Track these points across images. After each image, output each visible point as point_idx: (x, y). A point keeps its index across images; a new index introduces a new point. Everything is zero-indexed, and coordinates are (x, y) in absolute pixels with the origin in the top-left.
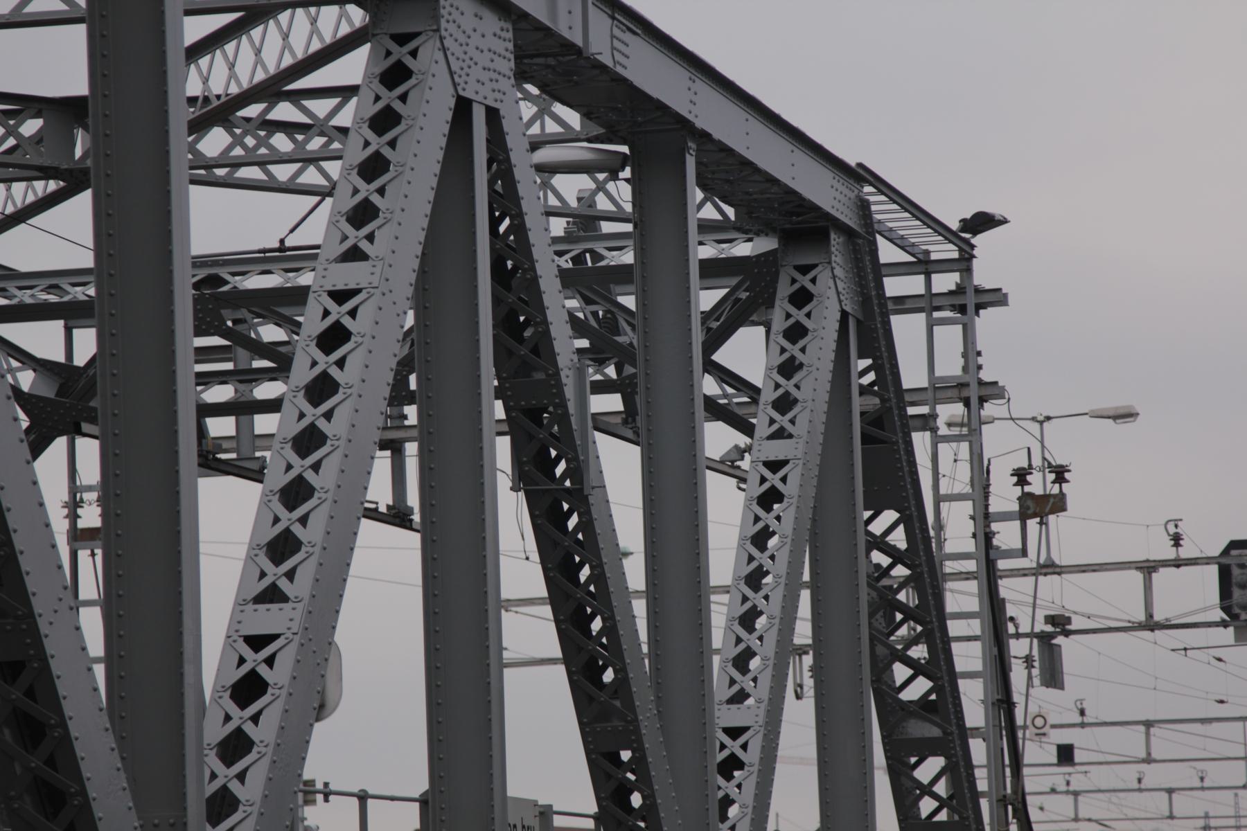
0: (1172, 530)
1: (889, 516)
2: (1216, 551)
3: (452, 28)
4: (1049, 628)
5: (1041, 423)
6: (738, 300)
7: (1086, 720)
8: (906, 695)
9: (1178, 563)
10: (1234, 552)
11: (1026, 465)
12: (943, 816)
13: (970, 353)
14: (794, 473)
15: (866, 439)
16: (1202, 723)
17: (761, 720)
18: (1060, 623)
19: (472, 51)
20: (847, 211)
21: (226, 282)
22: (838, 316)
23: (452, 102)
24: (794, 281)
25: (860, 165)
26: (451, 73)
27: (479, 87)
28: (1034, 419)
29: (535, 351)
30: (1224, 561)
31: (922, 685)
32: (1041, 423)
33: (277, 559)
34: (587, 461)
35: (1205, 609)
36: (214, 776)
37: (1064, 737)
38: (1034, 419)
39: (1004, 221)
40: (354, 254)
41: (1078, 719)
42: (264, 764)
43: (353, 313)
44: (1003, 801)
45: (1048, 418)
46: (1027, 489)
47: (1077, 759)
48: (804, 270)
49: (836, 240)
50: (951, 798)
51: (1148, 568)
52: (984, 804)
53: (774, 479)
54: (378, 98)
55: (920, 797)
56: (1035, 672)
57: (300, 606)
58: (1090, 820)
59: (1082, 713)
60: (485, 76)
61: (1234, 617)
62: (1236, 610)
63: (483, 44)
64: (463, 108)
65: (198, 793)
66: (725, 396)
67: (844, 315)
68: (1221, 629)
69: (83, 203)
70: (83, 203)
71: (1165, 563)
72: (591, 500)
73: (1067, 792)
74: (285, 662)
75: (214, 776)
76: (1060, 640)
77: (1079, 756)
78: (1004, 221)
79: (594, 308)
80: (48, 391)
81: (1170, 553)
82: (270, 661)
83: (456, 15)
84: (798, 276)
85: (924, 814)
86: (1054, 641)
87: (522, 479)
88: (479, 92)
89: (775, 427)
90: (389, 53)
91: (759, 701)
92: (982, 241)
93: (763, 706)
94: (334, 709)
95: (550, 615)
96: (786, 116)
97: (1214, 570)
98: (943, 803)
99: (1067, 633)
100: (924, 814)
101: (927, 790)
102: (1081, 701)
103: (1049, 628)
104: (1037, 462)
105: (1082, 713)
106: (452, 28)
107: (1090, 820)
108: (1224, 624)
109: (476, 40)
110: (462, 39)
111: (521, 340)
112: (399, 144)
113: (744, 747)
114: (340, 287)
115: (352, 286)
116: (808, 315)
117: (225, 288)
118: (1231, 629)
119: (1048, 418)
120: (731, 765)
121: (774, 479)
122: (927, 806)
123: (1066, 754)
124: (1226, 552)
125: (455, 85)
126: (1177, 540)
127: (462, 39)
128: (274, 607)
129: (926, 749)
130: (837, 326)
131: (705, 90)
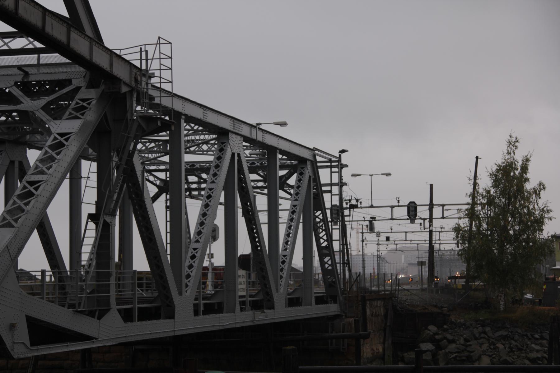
0: (398, 199)
1: (319, 212)
2: (407, 204)
3: (231, 141)
4: (371, 219)
5: (371, 176)
6: (291, 172)
7: (393, 231)
8: (323, 245)
9: (399, 206)
10: (411, 204)
11: (351, 199)
12: (330, 268)
13: (341, 178)
14: (298, 207)
15: (314, 198)
16: (362, 260)
17: (289, 254)
18: (373, 218)
19: (235, 144)
20: (311, 157)
21: (195, 166)
22: (308, 177)
23: (231, 154)
24: (300, 170)
25: (314, 148)
26: (231, 149)
27: (236, 150)
28: (370, 175)
29: (246, 193)
30: (409, 206)
31: (326, 243)
32: (371, 176)
33: (198, 235)
34: (255, 212)
35: (405, 216)
36: (187, 271)
37: (388, 235)
38: (370, 175)
39: (348, 151)
40: (213, 182)
41: (391, 231)
42: (195, 270)
43: (212, 193)
44: (344, 263)
45: (373, 175)
46: (351, 203)
47: (390, 240)
48: (302, 168)
49: (308, 163)
50: (331, 264)
51: (392, 207)
52: (338, 265)
53: (294, 209)
54: (218, 154)
55: (325, 264)
56: (368, 228)
57: (202, 244)
58: (399, 250)
59: (392, 229)
60: (237, 148)
61: (410, 218)
62: (411, 216)
63: (237, 143)
64: (233, 154)
65: (184, 274)
66: (289, 190)
67: (310, 177)
68: (407, 220)
69: (168, 156)
70: (168, 156)
71: (396, 206)
72: (256, 219)
73: (394, 244)
74: (199, 253)
75: (187, 271)
76: (374, 222)
77: (391, 239)
78: (348, 151)
79: (264, 172)
80: (162, 185)
81: (397, 204)
82: (197, 252)
83: (232, 138)
84: (301, 169)
85: (326, 267)
86: (373, 222)
87: (244, 215)
88: (236, 151)
89: (295, 198)
90: (220, 146)
91: (289, 250)
92: (343, 155)
93: (290, 251)
94: (217, 240)
95: (267, 214)
96: (297, 142)
97: (406, 208)
98: (330, 265)
99: (375, 220)
100: (326, 267)
101: (327, 263)
102: (392, 227)
103: (371, 219)
104: (353, 198)
105: (392, 229)
106: (231, 141)
107: (399, 250)
108: (408, 219)
109: (236, 142)
110: (233, 142)
111: (244, 191)
112: (217, 179)
113: (286, 259)
114: (210, 188)
115: (212, 188)
116: (303, 177)
117: (195, 167)
118: (409, 220)
119: (373, 175)
120: (283, 262)
121: (294, 209)
122: (327, 266)
123: (388, 239)
124: (409, 204)
125: (232, 151)
126: (398, 201)
127: (233, 142)
128: (198, 243)
129: (326, 255)
130: (308, 179)
131: (281, 141)
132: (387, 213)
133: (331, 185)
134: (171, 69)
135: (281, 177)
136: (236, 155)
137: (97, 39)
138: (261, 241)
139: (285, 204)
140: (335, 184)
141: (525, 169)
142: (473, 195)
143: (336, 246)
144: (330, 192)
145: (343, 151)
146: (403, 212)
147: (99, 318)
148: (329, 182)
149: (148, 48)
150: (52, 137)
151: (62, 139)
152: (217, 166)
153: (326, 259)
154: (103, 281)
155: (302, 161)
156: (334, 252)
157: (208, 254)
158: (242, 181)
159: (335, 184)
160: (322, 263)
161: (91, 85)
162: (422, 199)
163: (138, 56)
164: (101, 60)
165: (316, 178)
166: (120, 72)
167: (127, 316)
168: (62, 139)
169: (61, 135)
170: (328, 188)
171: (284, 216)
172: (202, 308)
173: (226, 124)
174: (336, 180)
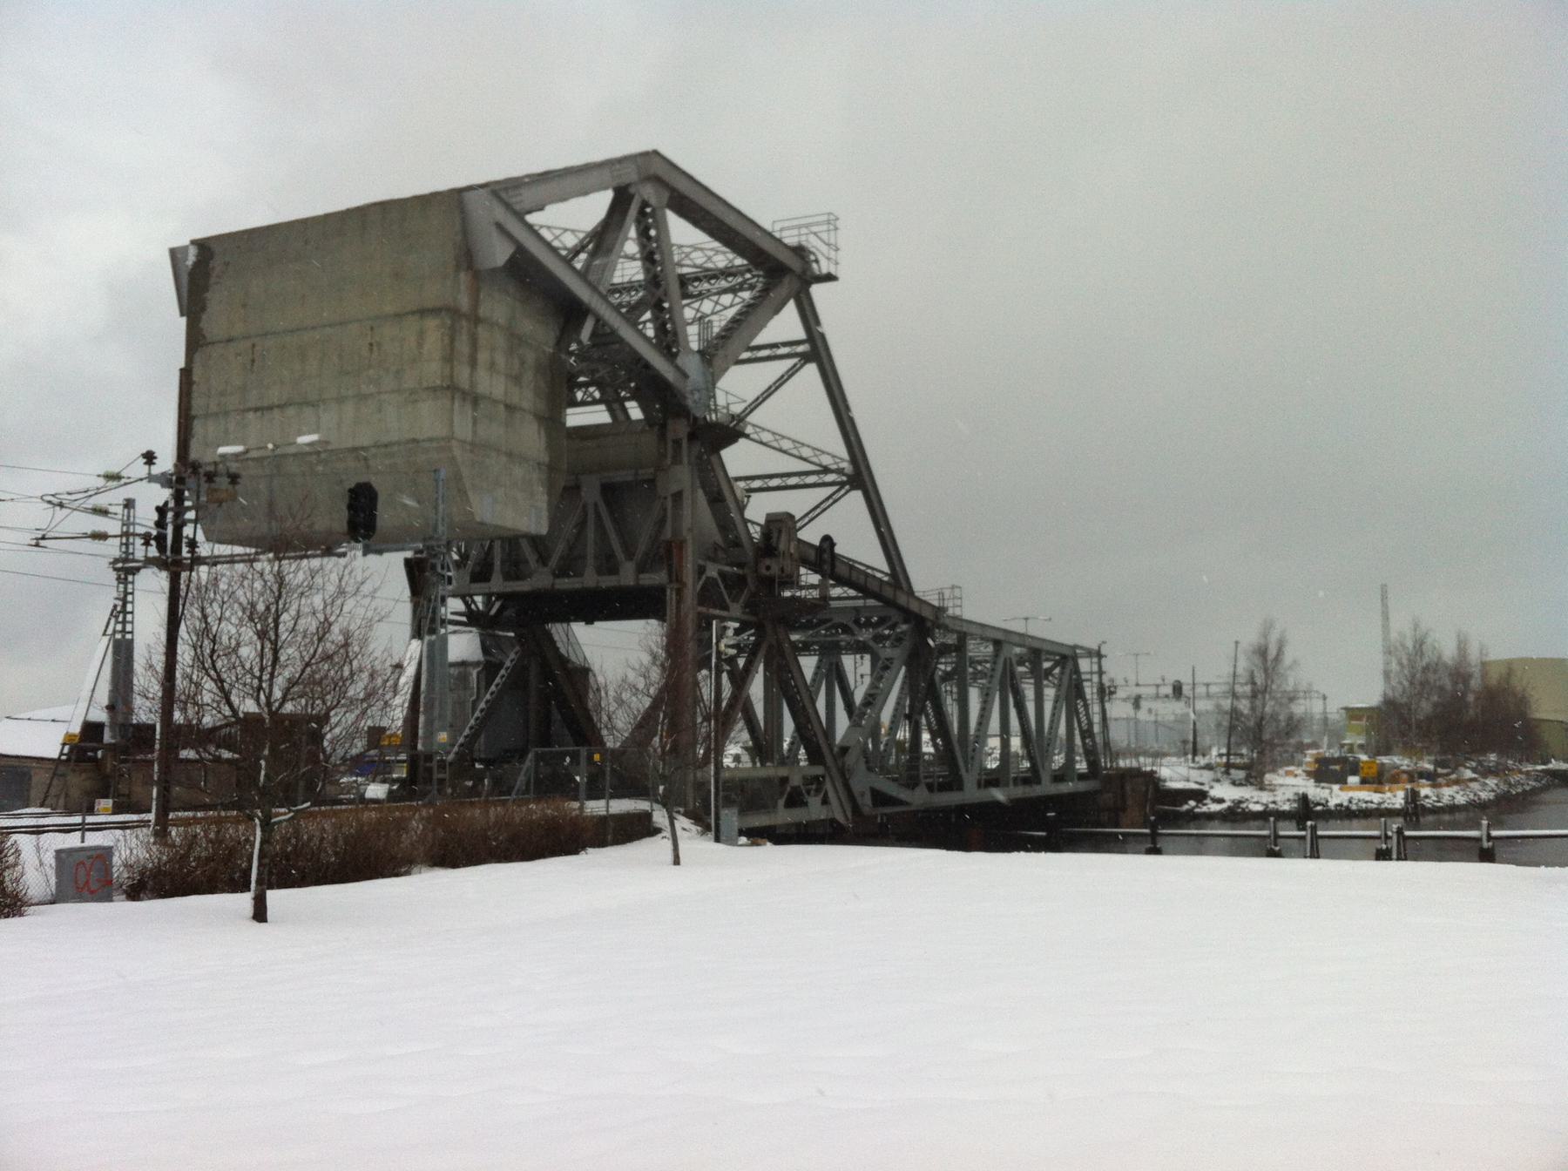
3: (785, 234)
13: (1100, 667)
64: (1005, 659)
132: (1152, 691)
133: (1091, 673)
134: (961, 598)
135: (1046, 670)
136: (1008, 661)
137: (910, 592)
138: (1029, 727)
139: (1050, 693)
140: (1095, 673)
141: (1280, 651)
142: (1235, 675)
143: (1096, 729)
144: (1090, 680)
145: (1104, 642)
146: (1168, 690)
147: (913, 789)
148: (1089, 670)
149: (944, 591)
150: (881, 662)
151: (888, 663)
152: (993, 670)
153: (1087, 741)
154: (716, 800)
155: (1064, 657)
156: (1094, 734)
157: (356, 781)
158: (1013, 675)
159: (1095, 673)
160: (1084, 744)
161: (906, 622)
162: (1186, 680)
163: (937, 597)
164: (914, 607)
165: (1076, 670)
166: (927, 613)
167: (930, 788)
168: (888, 663)
169: (887, 659)
170: (1088, 677)
171: (1048, 707)
172: (983, 782)
173: (999, 636)
174: (1095, 668)
